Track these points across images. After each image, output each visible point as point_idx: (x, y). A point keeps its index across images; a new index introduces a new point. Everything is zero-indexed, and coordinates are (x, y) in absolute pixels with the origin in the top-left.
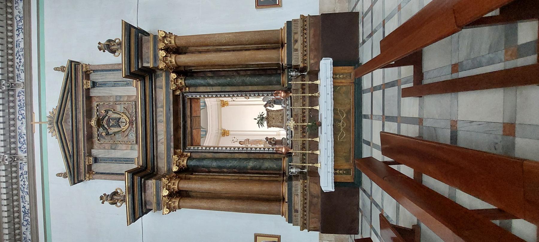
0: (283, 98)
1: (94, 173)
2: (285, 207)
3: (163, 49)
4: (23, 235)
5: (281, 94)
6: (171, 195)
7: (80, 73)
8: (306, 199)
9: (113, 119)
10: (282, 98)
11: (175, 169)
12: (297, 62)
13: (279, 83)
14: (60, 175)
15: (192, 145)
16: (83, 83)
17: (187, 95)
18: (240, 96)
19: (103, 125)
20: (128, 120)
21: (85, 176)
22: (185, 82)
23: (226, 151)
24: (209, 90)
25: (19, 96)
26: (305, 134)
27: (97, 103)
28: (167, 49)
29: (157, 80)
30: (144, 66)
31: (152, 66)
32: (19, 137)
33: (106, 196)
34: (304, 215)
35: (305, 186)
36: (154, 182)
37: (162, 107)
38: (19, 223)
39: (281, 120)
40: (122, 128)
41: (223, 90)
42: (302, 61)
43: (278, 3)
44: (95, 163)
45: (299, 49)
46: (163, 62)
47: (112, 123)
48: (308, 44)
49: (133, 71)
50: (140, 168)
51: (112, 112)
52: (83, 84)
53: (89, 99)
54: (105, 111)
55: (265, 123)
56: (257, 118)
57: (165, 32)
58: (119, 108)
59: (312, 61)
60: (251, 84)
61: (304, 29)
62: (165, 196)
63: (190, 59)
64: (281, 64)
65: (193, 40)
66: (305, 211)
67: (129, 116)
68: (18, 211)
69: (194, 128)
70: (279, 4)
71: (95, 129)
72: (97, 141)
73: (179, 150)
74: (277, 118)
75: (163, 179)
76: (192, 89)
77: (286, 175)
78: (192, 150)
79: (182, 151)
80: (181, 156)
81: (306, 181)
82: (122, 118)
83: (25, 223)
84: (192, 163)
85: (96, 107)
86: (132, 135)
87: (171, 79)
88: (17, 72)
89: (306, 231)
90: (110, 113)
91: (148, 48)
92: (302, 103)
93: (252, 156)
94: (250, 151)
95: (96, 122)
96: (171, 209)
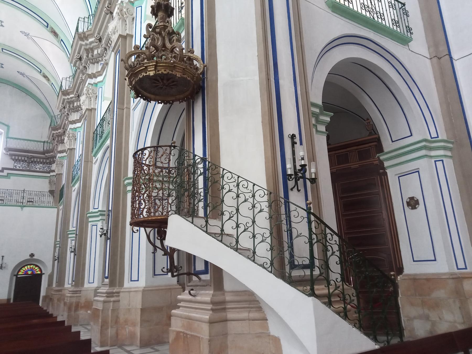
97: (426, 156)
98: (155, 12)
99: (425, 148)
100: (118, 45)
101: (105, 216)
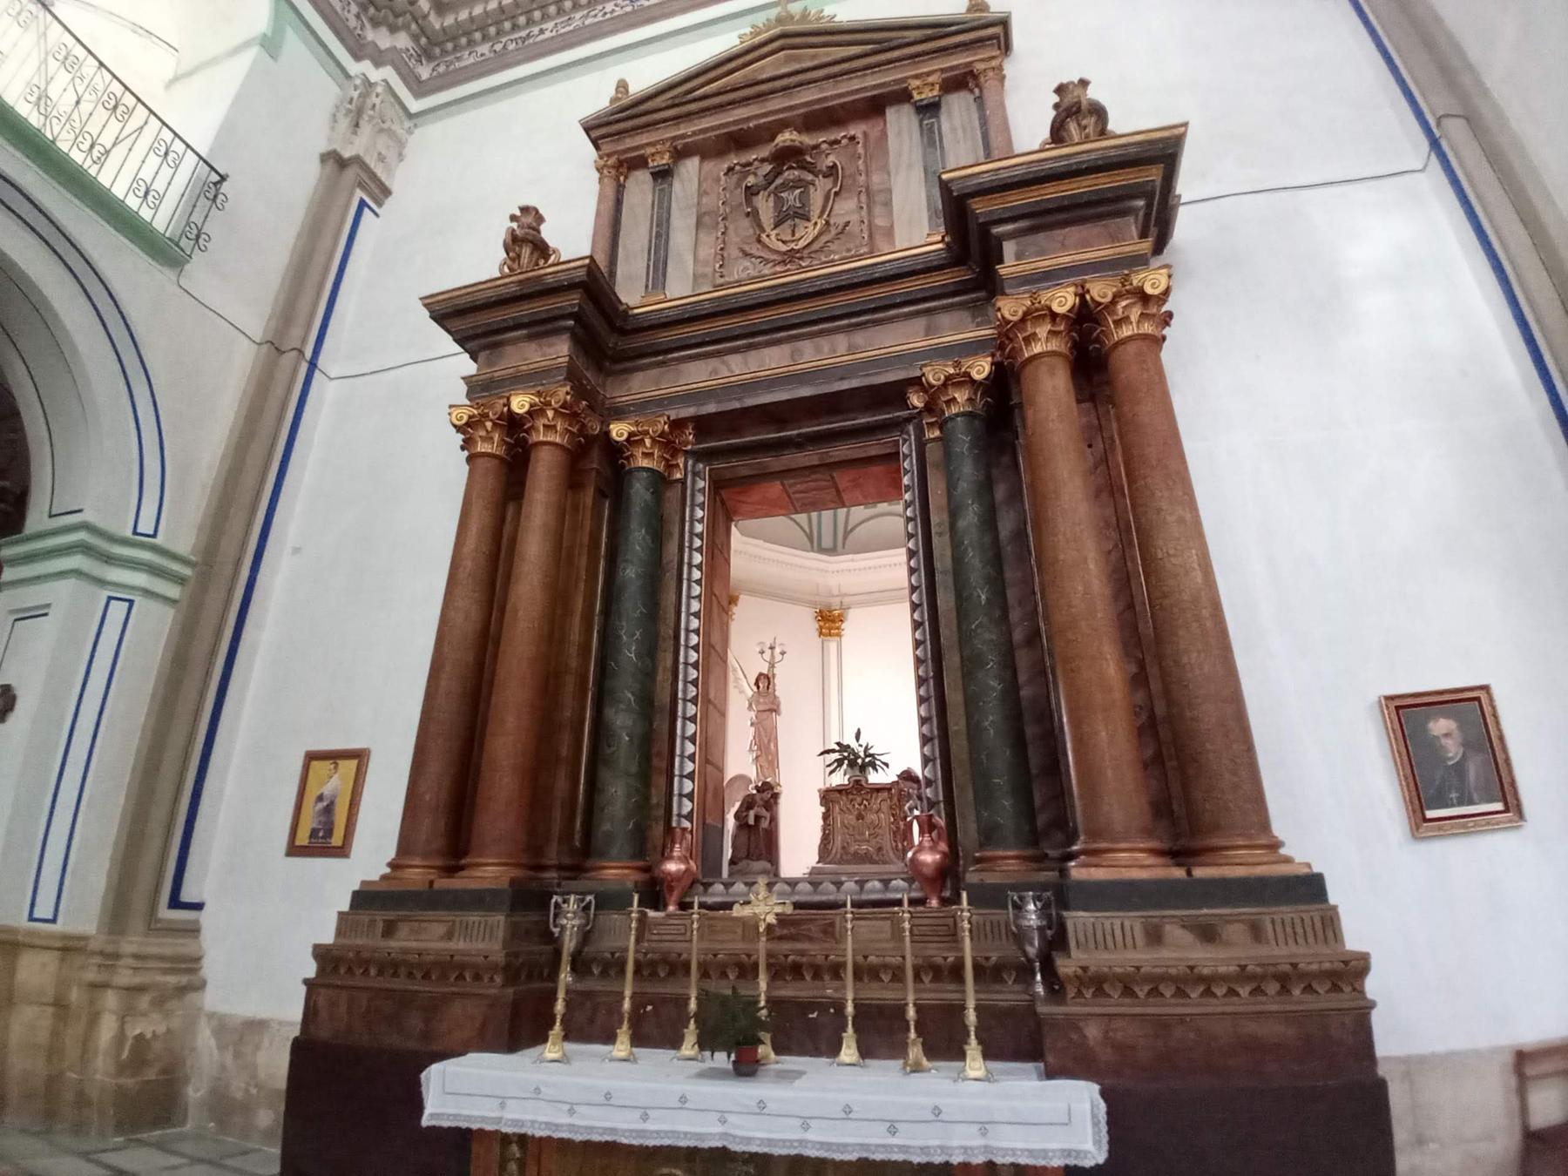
0: (913, 860)
1: (622, 178)
2: (416, 876)
3: (1082, 297)
5: (933, 849)
6: (513, 424)
7: (967, 57)
8: (426, 976)
9: (804, 198)
10: (910, 854)
11: (619, 431)
12: (1082, 939)
13: (988, 836)
14: (621, 89)
15: (718, 485)
16: (929, 74)
17: (910, 436)
18: (918, 652)
19: (780, 173)
20: (802, 244)
21: (609, 155)
22: (957, 415)
23: (683, 615)
24: (934, 519)
26: (731, 977)
27: (860, 136)
28: (1086, 318)
29: (965, 316)
30: (1004, 243)
31: (1003, 271)
33: (534, 224)
34: (365, 964)
35: (477, 977)
36: (560, 360)
37: (852, 350)
38: (499, 33)
39: (856, 853)
40: (773, 233)
41: (938, 577)
42: (1093, 969)
43: (1430, 814)
44: (652, 174)
45: (1166, 954)
46: (1025, 308)
47: (791, 197)
48: (1194, 1004)
49: (974, 206)
50: (617, 310)
51: (830, 190)
52: (924, 79)
53: (875, 107)
54: (832, 167)
55: (840, 779)
56: (863, 741)
57: (1167, 292)
58: (846, 208)
59: (1093, 1032)
60: (971, 702)
61: (1284, 981)
62: (508, 404)
63: (1054, 415)
64: (1075, 848)
65: (1145, 411)
66: (380, 973)
67: (816, 246)
68: (530, 22)
69: (790, 486)
70: (1426, 820)
71: (765, 151)
72: (726, 166)
73: (691, 437)
74: (864, 834)
75: (568, 388)
76: (934, 453)
77: (564, 883)
78: (694, 482)
79: (689, 447)
80: (668, 445)
81: (498, 979)
82: (807, 224)
83: (498, 47)
84: (639, 492)
85: (844, 137)
86: (746, 268)
87: (966, 363)
89: (310, 970)
90: (828, 183)
91: (1085, 244)
92: (885, 966)
93: (661, 725)
94: (680, 714)
95: (787, 144)
96: (467, 429)
97: (77, 573)
99: (85, 549)
100: (1118, 250)
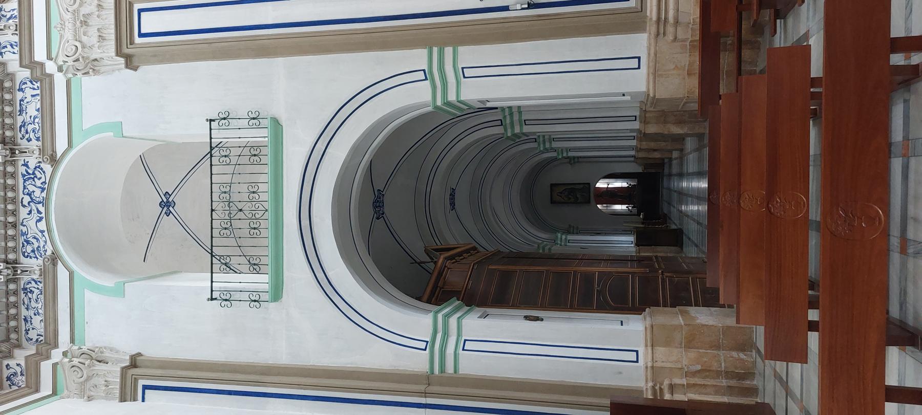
4: (21, 227)
25: (20, 90)
32: (23, 243)
38: (14, 201)
88: (24, 312)
98: (872, 238)
101: (737, 323)
